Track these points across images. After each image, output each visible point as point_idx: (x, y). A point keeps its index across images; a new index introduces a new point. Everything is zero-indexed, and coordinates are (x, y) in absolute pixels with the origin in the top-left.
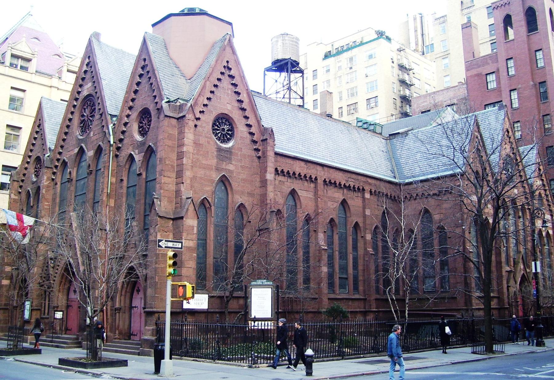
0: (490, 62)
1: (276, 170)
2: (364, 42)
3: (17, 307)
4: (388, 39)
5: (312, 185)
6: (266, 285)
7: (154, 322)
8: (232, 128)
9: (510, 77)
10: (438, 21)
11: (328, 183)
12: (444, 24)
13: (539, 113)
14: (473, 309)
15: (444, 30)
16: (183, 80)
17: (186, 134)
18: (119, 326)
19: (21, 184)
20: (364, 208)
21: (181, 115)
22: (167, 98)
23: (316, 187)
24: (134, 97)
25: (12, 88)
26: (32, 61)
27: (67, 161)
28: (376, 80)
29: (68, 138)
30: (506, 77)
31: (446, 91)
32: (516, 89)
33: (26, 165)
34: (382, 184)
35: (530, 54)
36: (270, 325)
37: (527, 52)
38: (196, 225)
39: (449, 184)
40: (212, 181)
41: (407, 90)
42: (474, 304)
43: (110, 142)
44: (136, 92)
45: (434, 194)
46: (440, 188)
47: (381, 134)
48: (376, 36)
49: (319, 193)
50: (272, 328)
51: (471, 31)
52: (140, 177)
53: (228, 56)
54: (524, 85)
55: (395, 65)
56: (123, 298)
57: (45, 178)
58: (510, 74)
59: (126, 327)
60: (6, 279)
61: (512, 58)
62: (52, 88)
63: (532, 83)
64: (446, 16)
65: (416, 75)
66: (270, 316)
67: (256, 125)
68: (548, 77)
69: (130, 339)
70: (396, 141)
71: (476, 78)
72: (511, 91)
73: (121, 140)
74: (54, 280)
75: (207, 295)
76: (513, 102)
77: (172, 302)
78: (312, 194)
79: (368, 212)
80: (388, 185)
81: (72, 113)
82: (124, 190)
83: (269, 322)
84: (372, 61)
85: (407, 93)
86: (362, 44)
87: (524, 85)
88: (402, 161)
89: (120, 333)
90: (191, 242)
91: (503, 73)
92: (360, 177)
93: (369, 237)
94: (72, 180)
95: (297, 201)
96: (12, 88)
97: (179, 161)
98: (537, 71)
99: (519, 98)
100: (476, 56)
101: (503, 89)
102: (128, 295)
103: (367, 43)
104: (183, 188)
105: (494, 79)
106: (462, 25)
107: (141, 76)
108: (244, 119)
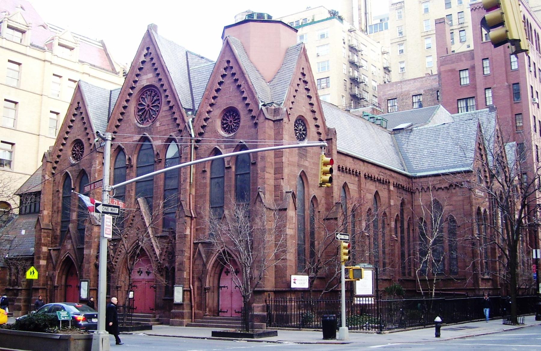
0: (464, 59)
1: (339, 167)
2: (315, 20)
3: (57, 287)
4: (341, 19)
5: (357, 179)
6: (367, 268)
7: (264, 299)
8: (306, 128)
9: (486, 76)
10: (395, 6)
11: (368, 177)
12: (401, 10)
13: (512, 112)
14: (480, 289)
15: (400, 17)
16: (264, 83)
17: (284, 136)
18: (208, 304)
19: (55, 165)
20: (389, 199)
21: (278, 118)
22: (262, 102)
23: (359, 180)
24: (216, 95)
25: (9, 61)
26: (27, 33)
27: (123, 147)
28: (328, 61)
29: (122, 124)
30: (482, 76)
31: (413, 81)
32: (490, 88)
33: (61, 147)
34: (401, 177)
35: (505, 57)
36: (371, 301)
37: (503, 55)
38: (294, 216)
39: (459, 178)
40: (295, 176)
41: (356, 72)
42: (480, 285)
43: (191, 135)
44: (218, 90)
45: (446, 188)
46: (452, 183)
47: (386, 128)
48: (329, 16)
49: (362, 186)
50: (373, 303)
51: (445, 27)
52: (229, 170)
53: (304, 64)
54: (499, 85)
55: (346, 46)
56: (211, 278)
57: (97, 162)
58: (485, 73)
59: (215, 304)
60: (43, 260)
61: (488, 58)
62: (46, 63)
63: (506, 84)
64: (403, 2)
65: (364, 57)
66: (371, 294)
67: (322, 125)
68: (521, 79)
69: (218, 315)
70: (401, 136)
71: (450, 73)
72: (486, 89)
73: (201, 134)
74: (116, 262)
75: (307, 277)
76: (487, 100)
77: (346, 282)
78: (357, 186)
79: (392, 204)
80: (404, 178)
81: (127, 101)
82: (208, 181)
83: (370, 299)
84: (323, 41)
85: (356, 74)
86: (313, 22)
87: (499, 85)
88: (410, 155)
89: (210, 311)
90: (292, 230)
91: (478, 72)
92: (387, 171)
93: (393, 224)
94: (132, 166)
95: (347, 193)
96: (9, 61)
97: (278, 160)
98: (512, 73)
99: (493, 96)
100: (450, 53)
101: (478, 87)
102: (217, 276)
103: (319, 22)
104: (283, 183)
105: (468, 75)
106: (436, 20)
107: (223, 76)
108: (313, 120)
